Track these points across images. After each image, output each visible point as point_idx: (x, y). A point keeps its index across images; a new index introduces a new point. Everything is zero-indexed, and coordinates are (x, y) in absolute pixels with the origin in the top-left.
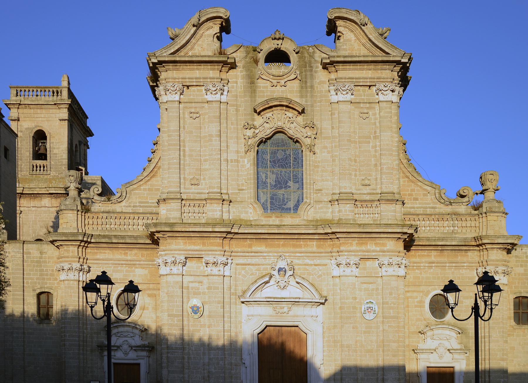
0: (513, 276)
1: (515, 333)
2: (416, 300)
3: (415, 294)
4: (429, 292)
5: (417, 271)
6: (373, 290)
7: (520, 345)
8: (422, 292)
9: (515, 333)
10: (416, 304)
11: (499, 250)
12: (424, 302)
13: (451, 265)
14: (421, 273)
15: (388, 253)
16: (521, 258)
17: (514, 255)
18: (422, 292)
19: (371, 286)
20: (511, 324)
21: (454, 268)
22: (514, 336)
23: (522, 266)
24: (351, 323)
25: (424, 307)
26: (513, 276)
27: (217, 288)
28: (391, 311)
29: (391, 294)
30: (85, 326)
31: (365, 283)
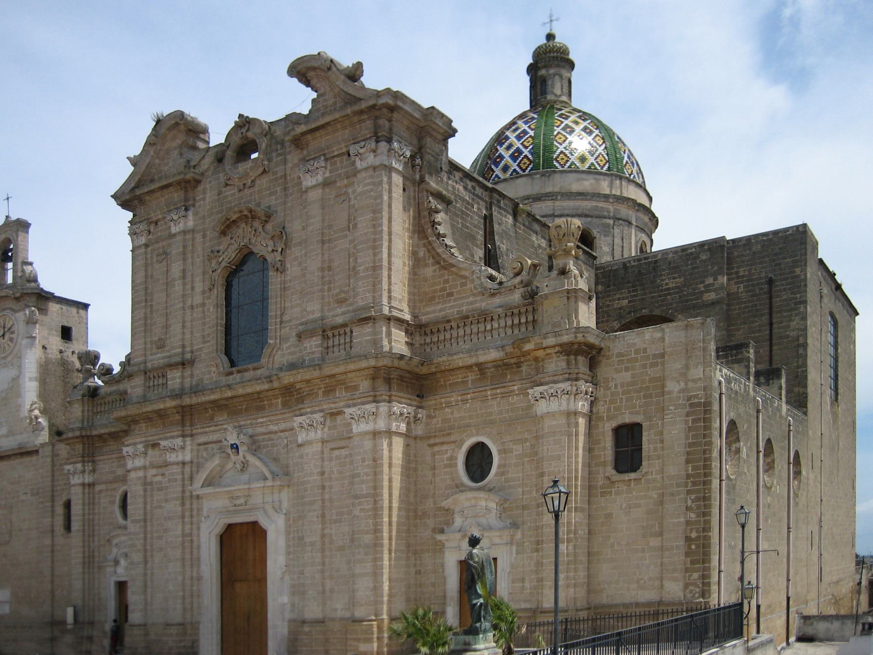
0: (613, 390)
1: (613, 490)
2: (445, 456)
3: (445, 447)
4: (462, 442)
5: (447, 410)
6: (346, 457)
7: (621, 509)
8: (454, 442)
9: (613, 490)
10: (445, 462)
11: (561, 356)
12: (456, 458)
13: (494, 391)
14: (452, 413)
15: (359, 401)
16: (626, 355)
17: (615, 352)
18: (454, 442)
19: (344, 452)
20: (606, 475)
21: (499, 396)
22: (611, 495)
23: (627, 369)
24: (315, 510)
25: (456, 465)
26: (613, 390)
27: (176, 480)
28: (364, 486)
29: (363, 461)
30: (91, 539)
31: (336, 449)
